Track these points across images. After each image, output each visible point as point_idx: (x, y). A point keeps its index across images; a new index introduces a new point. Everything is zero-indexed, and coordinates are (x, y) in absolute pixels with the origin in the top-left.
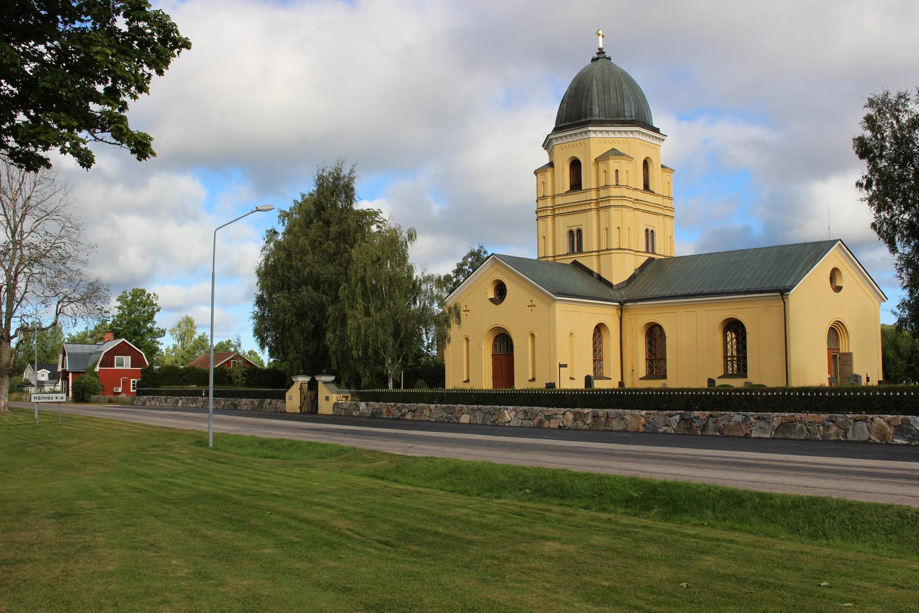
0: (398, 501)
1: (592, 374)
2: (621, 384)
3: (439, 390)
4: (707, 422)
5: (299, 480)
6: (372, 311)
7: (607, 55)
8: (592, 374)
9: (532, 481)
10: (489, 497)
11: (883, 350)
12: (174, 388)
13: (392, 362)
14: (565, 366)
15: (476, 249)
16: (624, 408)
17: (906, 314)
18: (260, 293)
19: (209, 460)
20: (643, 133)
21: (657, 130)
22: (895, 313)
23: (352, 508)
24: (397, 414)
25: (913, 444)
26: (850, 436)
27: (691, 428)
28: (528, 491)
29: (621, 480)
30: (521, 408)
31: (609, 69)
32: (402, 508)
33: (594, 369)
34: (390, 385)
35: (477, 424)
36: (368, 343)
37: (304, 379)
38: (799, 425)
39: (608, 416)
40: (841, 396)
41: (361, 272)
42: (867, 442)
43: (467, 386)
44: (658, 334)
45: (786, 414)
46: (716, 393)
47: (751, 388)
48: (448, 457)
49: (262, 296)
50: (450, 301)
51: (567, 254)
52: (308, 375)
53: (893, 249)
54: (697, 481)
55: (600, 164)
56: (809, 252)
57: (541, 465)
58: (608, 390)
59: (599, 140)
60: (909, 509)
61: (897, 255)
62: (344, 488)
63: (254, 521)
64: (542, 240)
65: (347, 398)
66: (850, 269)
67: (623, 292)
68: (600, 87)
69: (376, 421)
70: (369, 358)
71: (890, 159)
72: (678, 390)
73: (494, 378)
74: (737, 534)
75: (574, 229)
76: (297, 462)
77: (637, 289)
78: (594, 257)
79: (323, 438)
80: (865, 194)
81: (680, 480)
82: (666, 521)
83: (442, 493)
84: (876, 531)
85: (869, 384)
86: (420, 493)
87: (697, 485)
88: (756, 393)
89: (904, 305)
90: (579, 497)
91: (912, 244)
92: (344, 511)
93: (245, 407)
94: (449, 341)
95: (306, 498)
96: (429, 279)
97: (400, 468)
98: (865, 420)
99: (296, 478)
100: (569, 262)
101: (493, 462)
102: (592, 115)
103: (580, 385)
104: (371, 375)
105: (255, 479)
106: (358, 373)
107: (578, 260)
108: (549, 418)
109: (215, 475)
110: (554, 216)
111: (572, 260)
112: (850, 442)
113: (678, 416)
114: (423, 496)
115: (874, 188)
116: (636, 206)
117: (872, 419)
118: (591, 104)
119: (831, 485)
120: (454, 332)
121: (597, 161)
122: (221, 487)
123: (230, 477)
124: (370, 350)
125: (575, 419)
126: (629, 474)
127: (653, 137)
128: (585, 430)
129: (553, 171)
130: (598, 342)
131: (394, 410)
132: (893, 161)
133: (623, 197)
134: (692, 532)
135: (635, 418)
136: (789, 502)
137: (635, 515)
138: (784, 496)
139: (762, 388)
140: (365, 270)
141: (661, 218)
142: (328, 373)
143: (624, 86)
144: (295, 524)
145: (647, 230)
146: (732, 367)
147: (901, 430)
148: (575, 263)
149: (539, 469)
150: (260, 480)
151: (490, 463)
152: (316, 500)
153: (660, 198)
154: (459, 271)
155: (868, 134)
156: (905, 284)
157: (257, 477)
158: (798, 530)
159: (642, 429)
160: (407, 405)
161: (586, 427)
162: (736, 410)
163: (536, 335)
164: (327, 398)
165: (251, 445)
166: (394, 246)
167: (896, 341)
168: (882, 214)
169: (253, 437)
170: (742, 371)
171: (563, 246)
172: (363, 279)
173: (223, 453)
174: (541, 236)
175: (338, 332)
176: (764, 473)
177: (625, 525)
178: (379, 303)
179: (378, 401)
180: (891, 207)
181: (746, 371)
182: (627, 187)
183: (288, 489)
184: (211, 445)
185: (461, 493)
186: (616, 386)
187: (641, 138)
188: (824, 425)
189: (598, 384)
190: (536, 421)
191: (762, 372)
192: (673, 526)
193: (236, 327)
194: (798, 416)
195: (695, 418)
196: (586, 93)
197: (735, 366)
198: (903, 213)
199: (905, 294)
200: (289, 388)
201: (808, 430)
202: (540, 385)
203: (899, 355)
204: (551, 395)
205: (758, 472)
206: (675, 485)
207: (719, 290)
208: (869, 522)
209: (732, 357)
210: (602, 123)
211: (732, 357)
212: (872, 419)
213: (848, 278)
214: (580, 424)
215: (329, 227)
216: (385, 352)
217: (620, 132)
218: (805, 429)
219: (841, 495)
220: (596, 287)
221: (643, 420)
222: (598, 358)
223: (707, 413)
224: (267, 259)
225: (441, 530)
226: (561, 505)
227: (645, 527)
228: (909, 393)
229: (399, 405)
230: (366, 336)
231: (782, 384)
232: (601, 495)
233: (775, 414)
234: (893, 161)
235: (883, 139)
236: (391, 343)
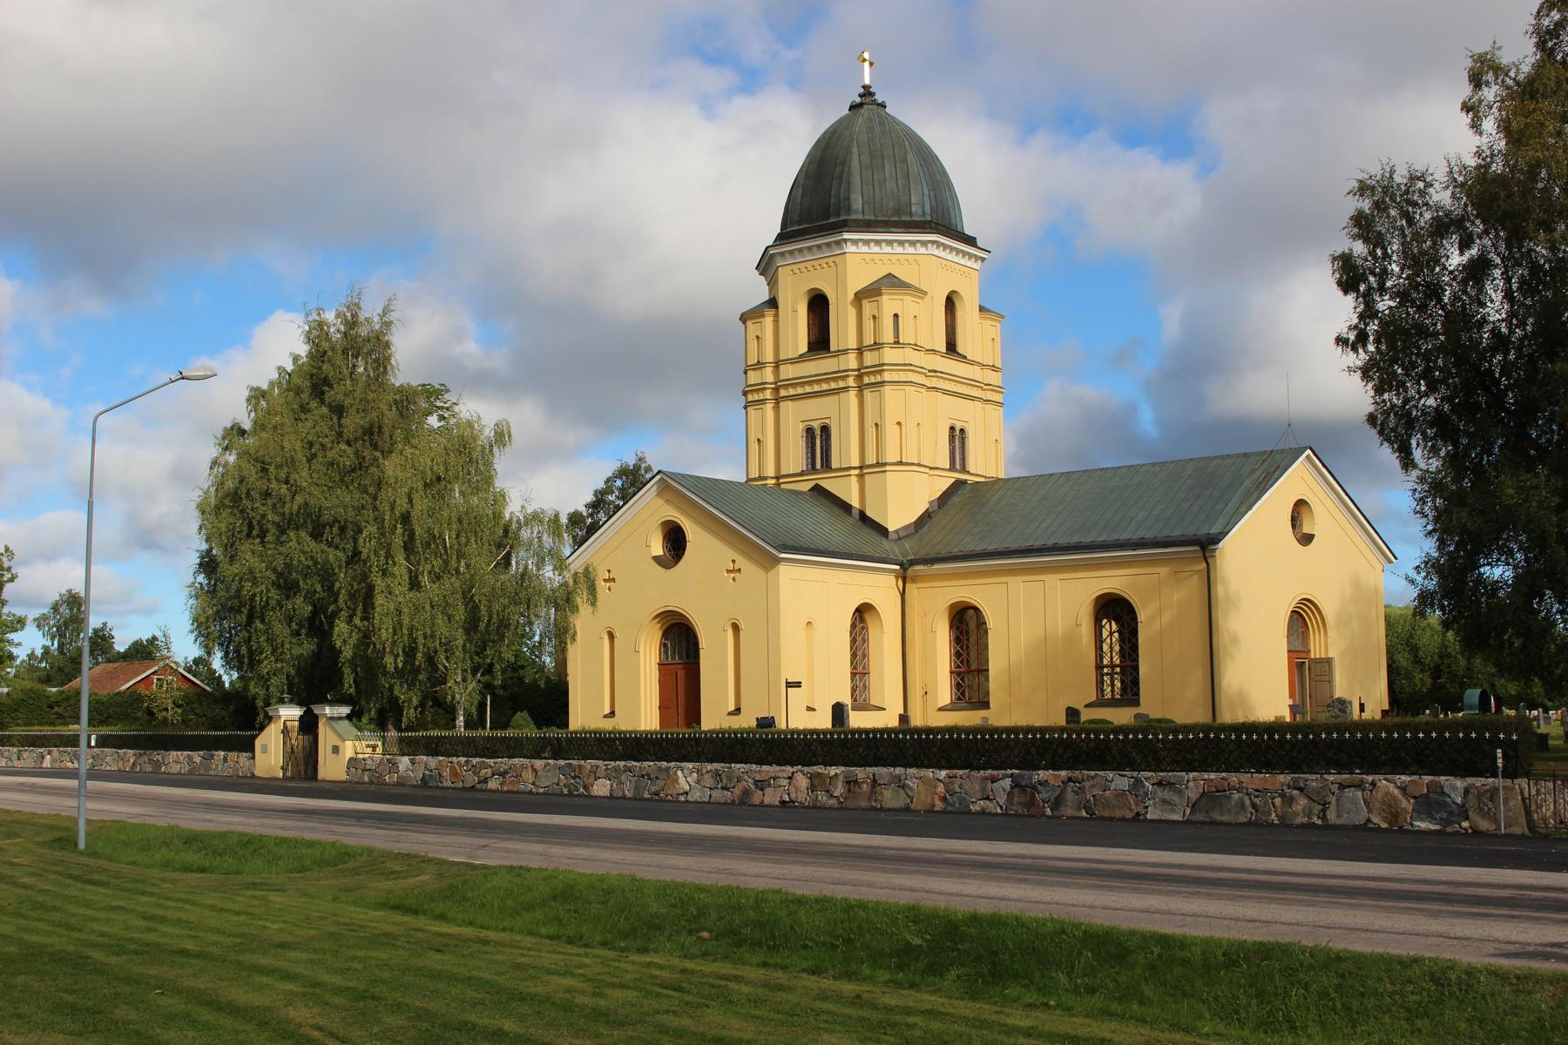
0: (434, 961)
1: (847, 700)
2: (904, 718)
3: (562, 734)
4: (1063, 791)
5: (242, 918)
6: (425, 580)
7: (879, 98)
8: (847, 700)
9: (714, 915)
10: (623, 950)
11: (1388, 652)
12: (36, 730)
13: (464, 680)
14: (798, 685)
15: (631, 462)
16: (906, 766)
17: (1432, 584)
18: (204, 546)
19: (70, 877)
20: (945, 247)
21: (971, 241)
22: (1412, 582)
23: (336, 980)
24: (471, 779)
25: (1449, 830)
26: (1332, 816)
27: (1032, 802)
28: (705, 934)
29: (890, 913)
30: (709, 767)
31: (882, 124)
32: (436, 976)
33: (853, 690)
34: (461, 720)
35: (624, 797)
36: (415, 641)
37: (290, 713)
38: (1236, 796)
39: (874, 781)
40: (1312, 744)
41: (402, 505)
42: (1365, 827)
43: (608, 725)
44: (972, 625)
45: (1213, 776)
46: (1079, 735)
47: (1146, 725)
48: (552, 866)
49: (210, 550)
50: (577, 562)
52: (300, 704)
53: (1407, 463)
54: (1037, 913)
55: (865, 303)
56: (1254, 470)
57: (734, 882)
58: (874, 731)
59: (862, 258)
60: (1452, 966)
61: (1415, 473)
62: (332, 934)
63: (122, 1011)
64: (754, 447)
65: (374, 748)
66: (1328, 503)
67: (907, 545)
68: (866, 159)
69: (428, 793)
70: (417, 671)
71: (1398, 294)
72: (1009, 730)
73: (663, 708)
74: (1114, 1025)
75: (816, 425)
76: (250, 879)
77: (936, 539)
78: (854, 479)
79: (314, 829)
80: (1358, 359)
81: (1005, 909)
82: (974, 1000)
83: (529, 941)
84: (1390, 1011)
85: (1366, 716)
86: (486, 942)
87: (1037, 920)
88: (1155, 735)
89: (1430, 565)
90: (805, 947)
91: (1443, 453)
92: (316, 985)
93: (175, 768)
94: (573, 639)
95: (242, 957)
96: (536, 517)
97: (458, 888)
98: (1359, 786)
99: (238, 913)
100: (805, 487)
101: (639, 875)
102: (849, 210)
103: (823, 721)
104: (422, 704)
105: (152, 918)
106: (397, 699)
107: (824, 484)
108: (761, 785)
109: (72, 909)
110: (778, 401)
111: (812, 484)
112: (1334, 827)
113: (1008, 781)
114: (489, 949)
115: (1371, 348)
116: (933, 382)
117: (1373, 784)
118: (848, 190)
119: (1300, 917)
120: (584, 621)
121: (860, 297)
122: (76, 935)
123: (101, 915)
124: (419, 655)
125: (813, 788)
126: (904, 899)
127: (964, 254)
128: (831, 808)
129: (776, 316)
130: (859, 639)
131: (463, 771)
132: (1403, 296)
133: (906, 366)
134: (1023, 1023)
135: (925, 784)
136: (1219, 954)
137: (912, 986)
138: (1207, 942)
139: (1166, 725)
140: (410, 501)
141: (978, 404)
143: (910, 157)
144: (205, 1015)
145: (952, 429)
146: (1113, 685)
147: (1429, 804)
148: (818, 490)
149: (728, 891)
150: (163, 920)
151: (633, 879)
152: (264, 961)
153: (977, 368)
154: (598, 503)
155: (1359, 248)
156: (1430, 527)
157: (159, 912)
158: (1237, 1013)
159: (939, 805)
160: (491, 762)
161: (833, 802)
162: (1118, 767)
163: (742, 626)
164: (336, 750)
165: (166, 844)
166: (470, 457)
167: (1411, 636)
168: (1386, 396)
169: (172, 828)
170: (1130, 693)
171: (795, 459)
172: (406, 518)
173: (105, 864)
174: (753, 439)
175: (357, 621)
176: (1169, 893)
177: (889, 1009)
178: (437, 563)
179: (435, 753)
180: (1402, 385)
182: (916, 347)
183: (216, 937)
184: (82, 846)
185: (570, 941)
186: (894, 723)
187: (943, 254)
188: (1283, 796)
189: (858, 720)
190: (737, 791)
191: (1169, 697)
192: (985, 1010)
193: (156, 607)
194: (1234, 778)
195: (1040, 783)
196: (839, 169)
197: (1118, 684)
198: (1427, 395)
199: (1430, 546)
200: (262, 728)
201: (1254, 805)
202: (747, 721)
203: (1417, 661)
204: (766, 741)
205: (1158, 892)
206: (996, 921)
207: (1089, 539)
208: (1376, 994)
209: (1112, 666)
210: (868, 226)
211: (1112, 666)
212: (1373, 784)
213: (1326, 517)
214: (822, 797)
215: (340, 417)
216: (447, 659)
217: (901, 243)
218: (1248, 802)
219: (1321, 940)
220: (860, 536)
221: (941, 789)
222: (860, 669)
223: (1063, 773)
224: (220, 484)
225: (508, 1025)
226: (765, 965)
227: (931, 1013)
228: (1440, 734)
229: (475, 761)
230: (411, 629)
231: (1200, 716)
232: (848, 941)
233: (1192, 775)
234: (1403, 296)
235: (1386, 256)
236: (460, 642)
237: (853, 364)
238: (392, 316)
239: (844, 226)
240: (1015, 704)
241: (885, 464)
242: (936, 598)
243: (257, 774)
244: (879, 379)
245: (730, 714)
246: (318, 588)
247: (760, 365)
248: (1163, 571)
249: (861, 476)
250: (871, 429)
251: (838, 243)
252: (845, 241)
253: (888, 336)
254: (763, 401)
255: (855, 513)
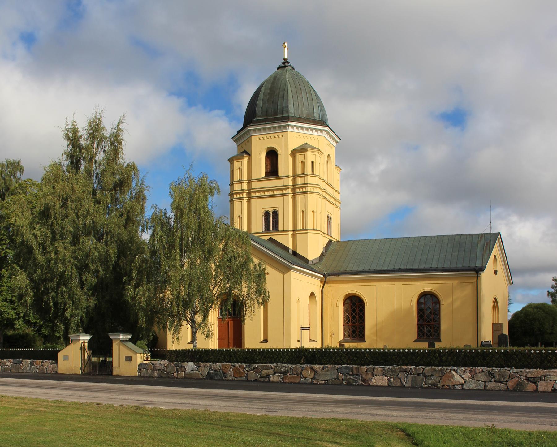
51: (262, 233)
55: (235, 162)
75: (271, 211)
78: (290, 236)
100: (266, 238)
102: (288, 112)
103: (337, 346)
107: (274, 237)
110: (250, 198)
111: (268, 237)
121: (294, 153)
133: (316, 186)
142: (125, 332)
148: (271, 240)
164: (129, 359)
171: (258, 226)
181: (439, 335)
196: (281, 93)
210: (298, 120)
237: (291, 183)
238: (122, 126)
239: (287, 119)
240: (373, 341)
241: (307, 230)
243: (60, 371)
245: (261, 342)
246: (101, 269)
247: (240, 181)
248: (455, 282)
250: (300, 214)
251: (285, 127)
252: (289, 125)
253: (309, 171)
254: (243, 198)
255: (291, 252)
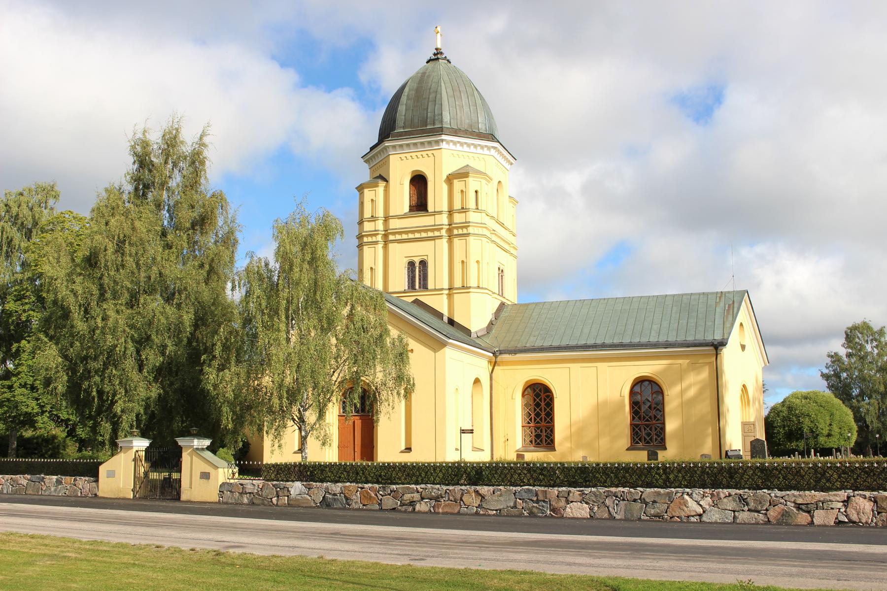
51: (405, 292)
55: (456, 182)
59: (446, 157)
75: (417, 260)
78: (445, 297)
100: (410, 300)
102: (441, 122)
107: (420, 298)
110: (386, 242)
121: (450, 180)
133: (482, 225)
135: (500, 498)
142: (200, 435)
148: (417, 302)
164: (205, 476)
171: (399, 281)
210: (456, 132)
238: (206, 140)
239: (440, 131)
240: (568, 449)
241: (470, 287)
242: (516, 376)
243: (100, 494)
244: (465, 231)
246: (169, 343)
248: (684, 362)
249: (450, 296)
251: (437, 142)
252: (442, 140)
253: (471, 204)
254: (376, 243)
